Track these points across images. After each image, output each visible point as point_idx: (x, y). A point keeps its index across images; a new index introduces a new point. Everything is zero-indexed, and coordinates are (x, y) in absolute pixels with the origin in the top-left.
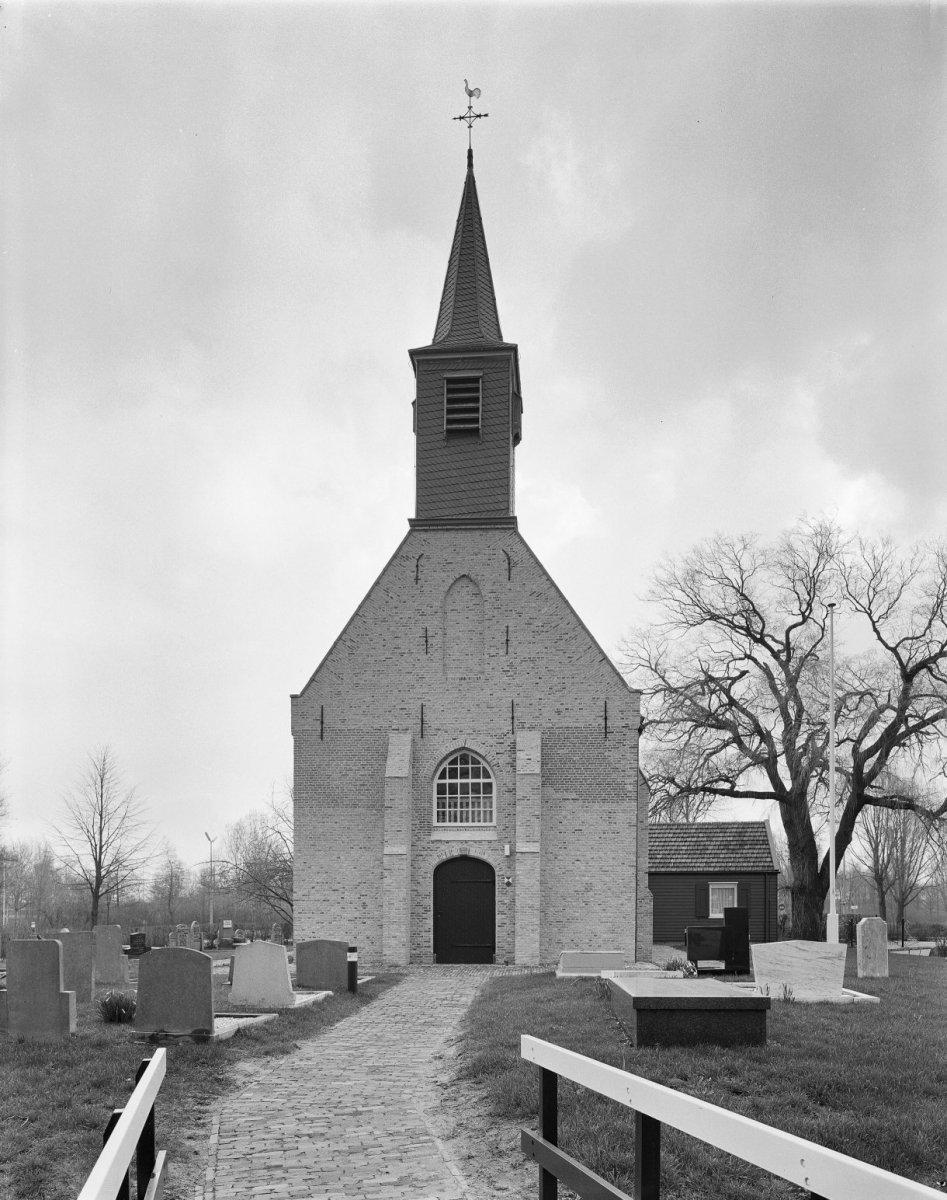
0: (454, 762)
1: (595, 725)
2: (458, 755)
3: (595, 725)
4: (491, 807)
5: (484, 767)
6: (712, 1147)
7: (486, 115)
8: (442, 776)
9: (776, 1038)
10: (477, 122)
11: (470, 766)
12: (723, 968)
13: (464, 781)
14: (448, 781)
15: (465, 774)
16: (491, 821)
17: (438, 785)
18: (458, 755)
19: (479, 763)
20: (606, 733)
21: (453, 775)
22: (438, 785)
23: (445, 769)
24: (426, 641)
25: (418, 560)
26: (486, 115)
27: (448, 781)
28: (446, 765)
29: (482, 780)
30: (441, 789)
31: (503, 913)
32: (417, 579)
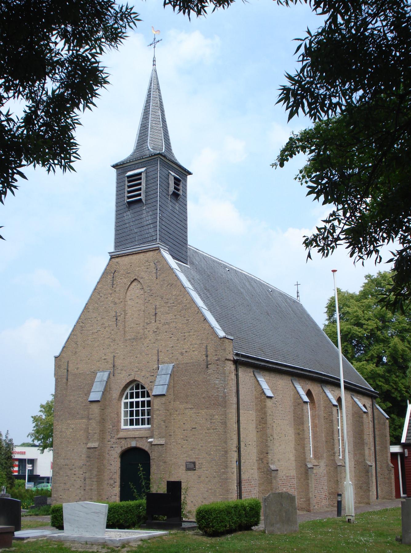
8: (126, 398)
11: (140, 390)
32: (113, 284)
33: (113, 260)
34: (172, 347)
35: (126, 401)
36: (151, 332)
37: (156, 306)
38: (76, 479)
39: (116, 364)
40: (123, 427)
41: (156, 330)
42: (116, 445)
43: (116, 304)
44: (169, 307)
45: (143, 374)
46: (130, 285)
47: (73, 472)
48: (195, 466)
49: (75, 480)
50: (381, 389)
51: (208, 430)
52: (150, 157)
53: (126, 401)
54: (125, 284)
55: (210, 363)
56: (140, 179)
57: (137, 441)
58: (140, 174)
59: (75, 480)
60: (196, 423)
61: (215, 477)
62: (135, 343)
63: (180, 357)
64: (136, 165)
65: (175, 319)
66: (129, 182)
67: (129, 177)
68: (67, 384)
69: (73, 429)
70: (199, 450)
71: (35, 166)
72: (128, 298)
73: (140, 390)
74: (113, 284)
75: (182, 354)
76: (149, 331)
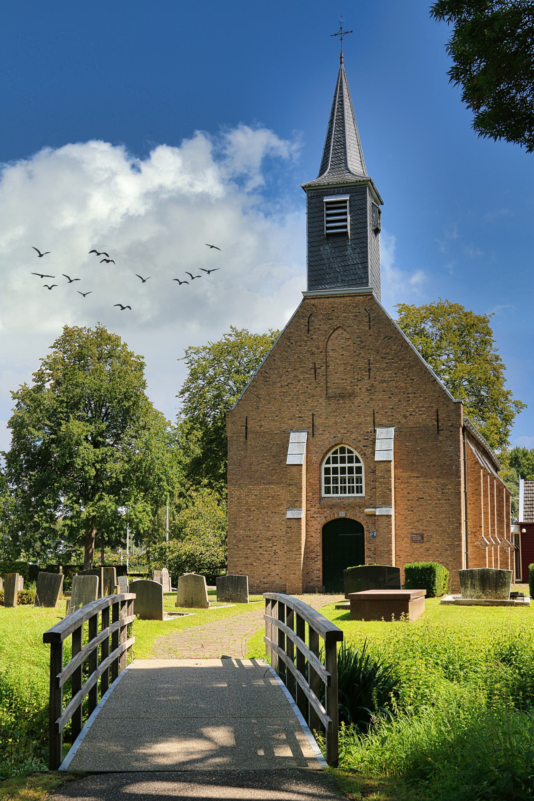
0: (336, 452)
1: (430, 424)
2: (338, 447)
3: (430, 424)
4: (361, 483)
5: (356, 456)
6: (319, 592)
7: (351, 32)
8: (328, 462)
9: (300, 461)
10: (345, 37)
11: (346, 455)
12: (303, 436)
13: (343, 465)
14: (331, 466)
15: (343, 460)
16: (361, 493)
17: (325, 468)
18: (338, 447)
19: (352, 453)
20: (438, 430)
21: (335, 461)
22: (325, 468)
23: (329, 457)
24: (315, 372)
25: (309, 318)
26: (351, 32)
27: (331, 466)
28: (330, 455)
29: (354, 465)
30: (327, 471)
31: (369, 557)
32: (309, 330)
33: (307, 301)
34: (393, 408)
35: (328, 466)
36: (364, 390)
37: (369, 360)
38: (263, 552)
39: (316, 424)
40: (324, 495)
41: (369, 388)
42: (319, 515)
43: (313, 354)
44: (386, 363)
45: (353, 436)
46: (332, 333)
47: (258, 544)
48: (422, 538)
49: (261, 554)
50: (137, 528)
51: (439, 500)
52: (344, 183)
53: (328, 466)
54: (326, 331)
55: (441, 428)
56: (345, 207)
57: (347, 510)
58: (345, 202)
59: (261, 554)
60: (424, 493)
61: (447, 550)
62: (341, 401)
63: (403, 421)
64: (336, 190)
65: (397, 377)
66: (328, 209)
67: (327, 203)
68: (246, 443)
69: (256, 495)
70: (427, 521)
71: (468, 107)
72: (329, 348)
73: (346, 455)
74: (309, 330)
75: (405, 417)
76: (360, 389)
